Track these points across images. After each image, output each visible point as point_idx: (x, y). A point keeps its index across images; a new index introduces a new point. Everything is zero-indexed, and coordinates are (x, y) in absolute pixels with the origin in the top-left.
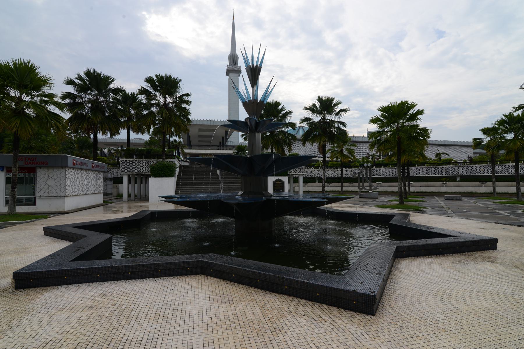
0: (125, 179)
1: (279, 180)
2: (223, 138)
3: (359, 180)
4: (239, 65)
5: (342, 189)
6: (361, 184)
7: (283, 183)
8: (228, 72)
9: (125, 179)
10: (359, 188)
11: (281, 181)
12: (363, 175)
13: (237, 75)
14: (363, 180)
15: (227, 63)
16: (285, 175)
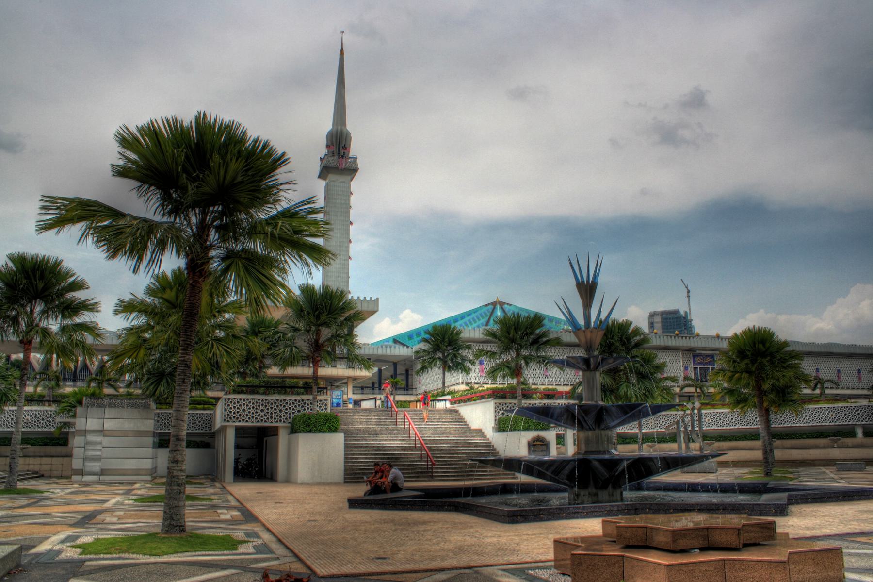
8: (325, 171)
13: (349, 178)
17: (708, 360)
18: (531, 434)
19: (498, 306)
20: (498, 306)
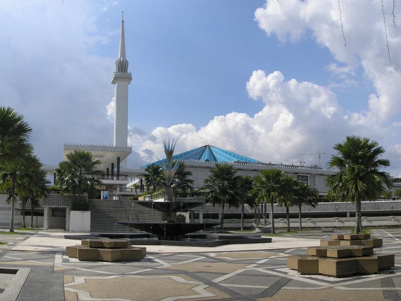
4: (129, 71)
8: (116, 79)
11: (183, 216)
12: (259, 211)
14: (259, 217)
15: (114, 69)
16: (186, 211)
17: (304, 179)
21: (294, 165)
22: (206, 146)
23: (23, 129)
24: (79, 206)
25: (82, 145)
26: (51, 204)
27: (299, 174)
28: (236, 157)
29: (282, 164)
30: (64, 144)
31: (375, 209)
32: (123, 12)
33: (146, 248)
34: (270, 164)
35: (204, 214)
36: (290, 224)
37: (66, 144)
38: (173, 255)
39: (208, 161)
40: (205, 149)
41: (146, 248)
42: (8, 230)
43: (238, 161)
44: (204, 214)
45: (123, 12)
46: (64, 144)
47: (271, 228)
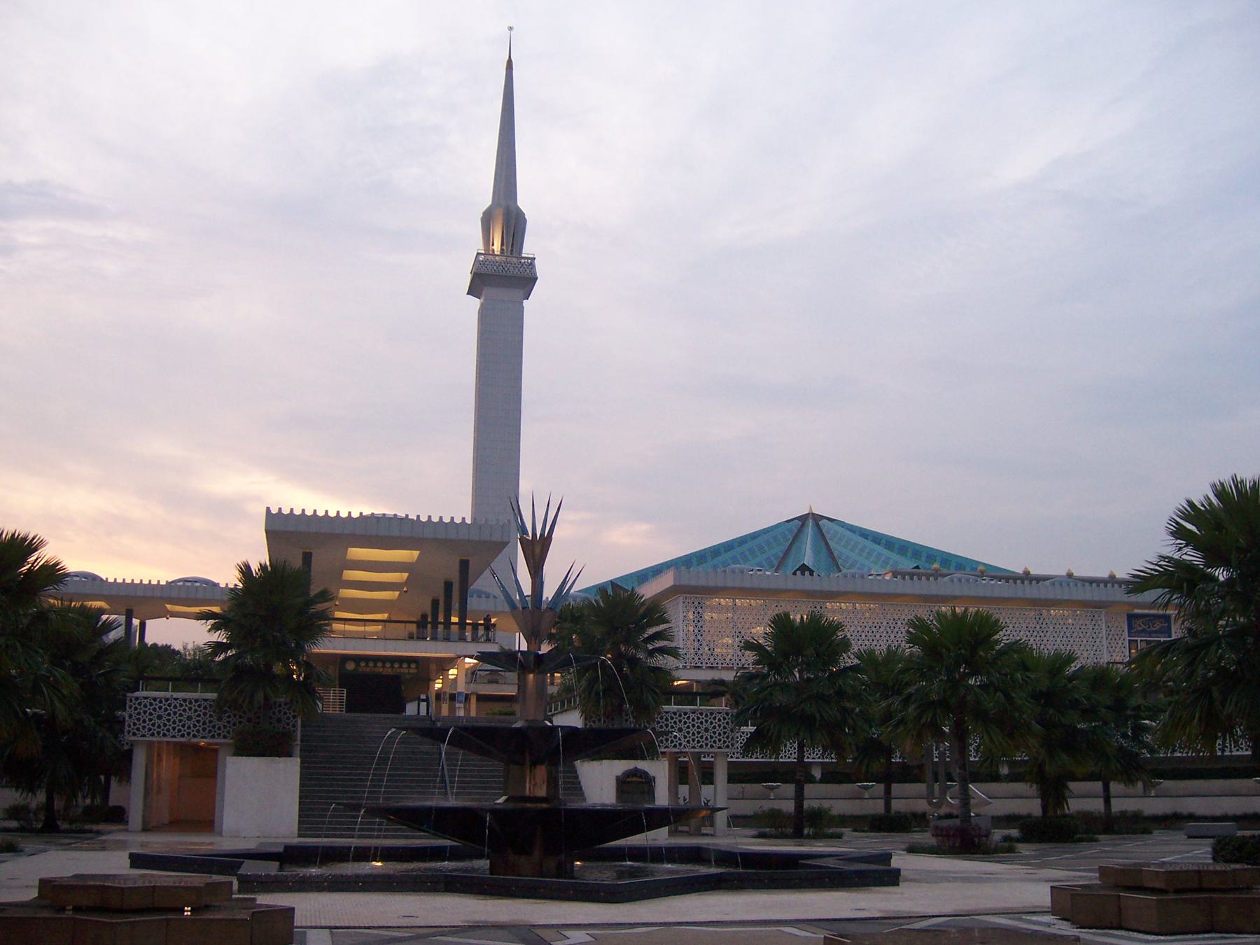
0: (721, 774)
1: (635, 772)
2: (448, 586)
3: (929, 776)
5: (888, 806)
6: (937, 786)
7: (647, 782)
8: (481, 281)
9: (721, 774)
10: (930, 803)
14: (694, 773)
17: (1158, 626)
18: (621, 766)
19: (810, 522)
20: (810, 522)
21: (1032, 572)
22: (803, 519)
23: (810, 522)
24: (264, 743)
25: (446, 520)
26: (159, 733)
27: (1137, 611)
28: (909, 554)
29: (1070, 575)
30: (268, 509)
31: (194, 706)
32: (511, 29)
33: (291, 910)
34: (1027, 577)
35: (731, 765)
36: (1113, 801)
37: (274, 511)
38: (418, 937)
39: (811, 573)
40: (803, 525)
41: (291, 910)
42: (790, 831)
43: (917, 567)
44: (731, 765)
45: (511, 29)
46: (268, 509)
47: (207, 823)
